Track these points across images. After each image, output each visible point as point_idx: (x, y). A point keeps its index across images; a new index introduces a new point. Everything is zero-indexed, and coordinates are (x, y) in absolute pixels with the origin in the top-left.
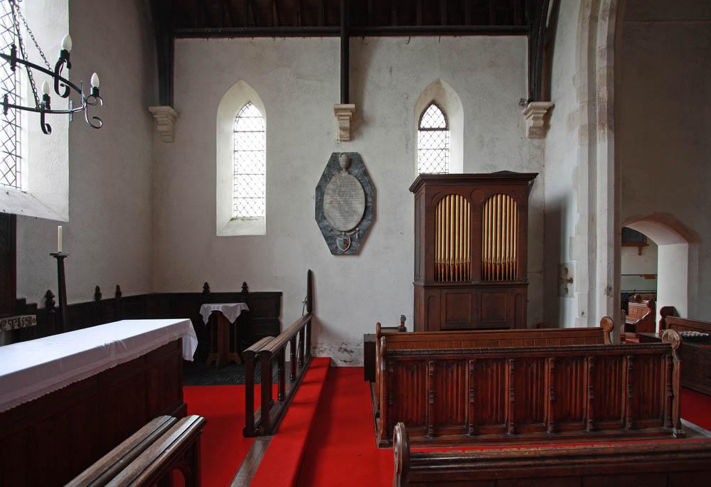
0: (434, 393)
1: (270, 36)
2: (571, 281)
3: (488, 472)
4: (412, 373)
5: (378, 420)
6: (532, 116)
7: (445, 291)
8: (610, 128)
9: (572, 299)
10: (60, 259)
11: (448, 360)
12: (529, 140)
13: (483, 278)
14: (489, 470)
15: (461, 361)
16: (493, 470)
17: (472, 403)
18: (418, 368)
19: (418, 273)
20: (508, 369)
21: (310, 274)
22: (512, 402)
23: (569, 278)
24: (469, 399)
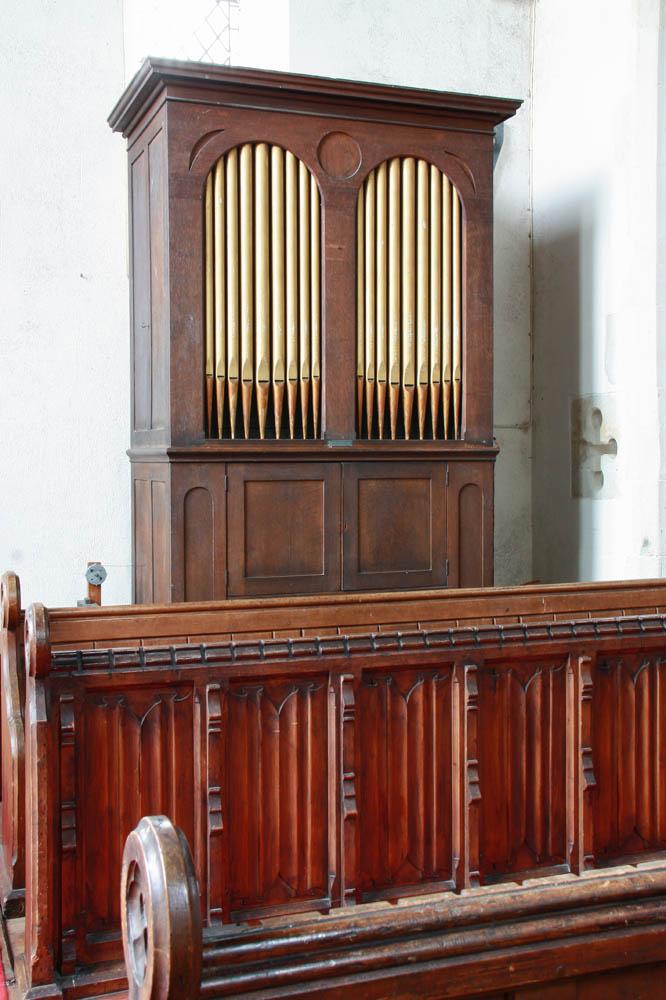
0: (226, 796)
3: (486, 964)
4: (146, 732)
5: (17, 925)
7: (240, 471)
11: (267, 677)
13: (361, 432)
14: (486, 957)
15: (311, 679)
16: (500, 955)
17: (350, 817)
18: (164, 708)
19: (144, 415)
20: (461, 695)
22: (474, 803)
23: (604, 440)
24: (342, 803)
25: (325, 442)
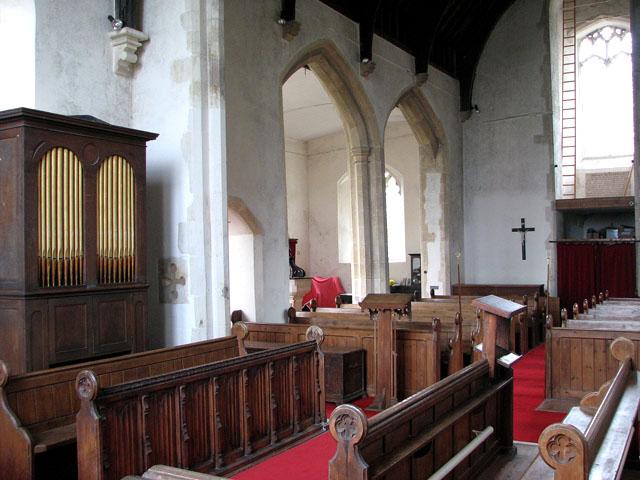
1: (636, 150)
2: (183, 281)
6: (125, 45)
8: (222, 94)
9: (185, 305)
10: (292, 243)
12: (116, 76)
15: (170, 389)
21: (524, 258)
22: (149, 454)
25: (85, 286)
